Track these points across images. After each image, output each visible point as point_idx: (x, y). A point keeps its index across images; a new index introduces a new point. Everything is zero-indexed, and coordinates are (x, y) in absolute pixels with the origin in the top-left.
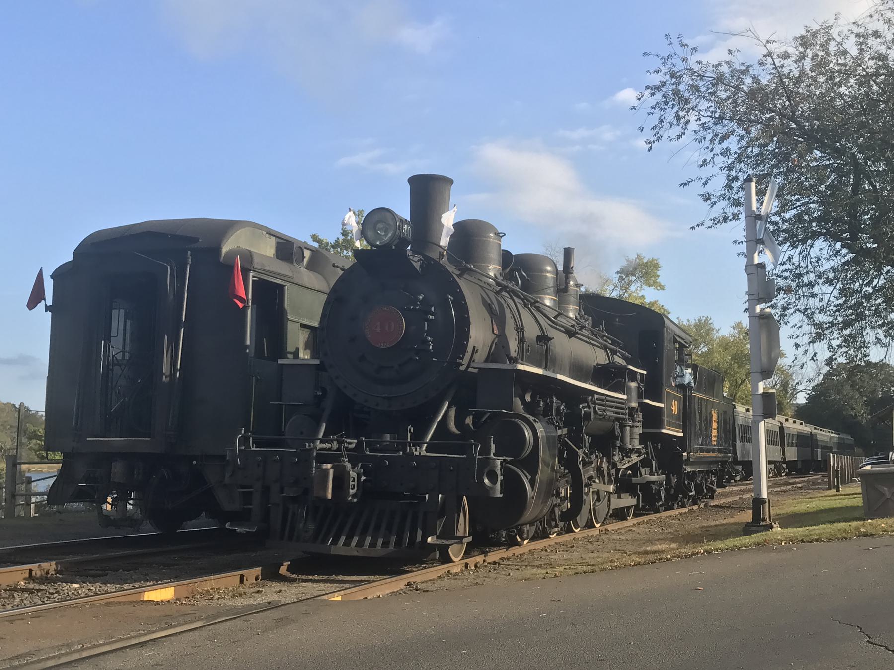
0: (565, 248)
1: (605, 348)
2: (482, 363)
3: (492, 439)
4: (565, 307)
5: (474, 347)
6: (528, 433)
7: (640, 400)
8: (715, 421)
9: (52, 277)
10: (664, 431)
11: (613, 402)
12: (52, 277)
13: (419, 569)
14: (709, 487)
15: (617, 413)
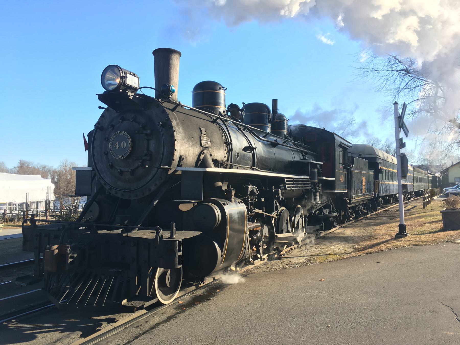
0: (272, 100)
1: (301, 152)
2: (193, 167)
3: (174, 225)
4: (282, 131)
5: (181, 157)
6: (218, 212)
7: (320, 178)
8: (364, 182)
9: (88, 136)
10: (336, 191)
11: (299, 181)
12: (88, 136)
13: (378, 157)
14: (362, 211)
15: (302, 187)
